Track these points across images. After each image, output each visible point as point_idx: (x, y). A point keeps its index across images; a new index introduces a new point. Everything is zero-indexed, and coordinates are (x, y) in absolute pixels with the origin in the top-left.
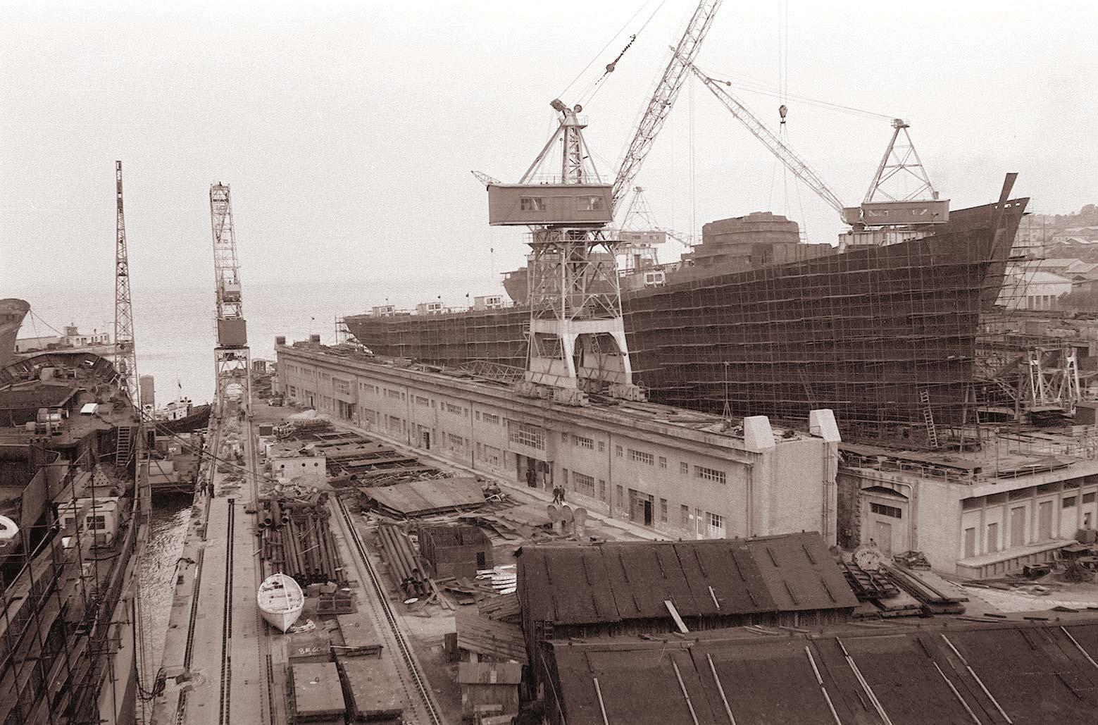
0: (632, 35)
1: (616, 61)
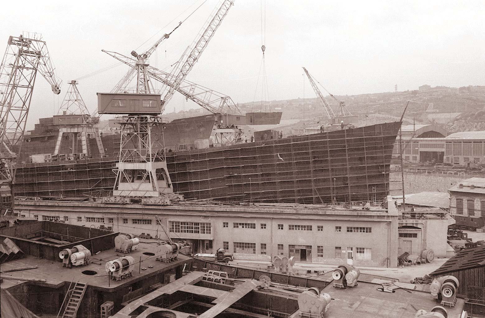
0: (180, 22)
1: (170, 33)
